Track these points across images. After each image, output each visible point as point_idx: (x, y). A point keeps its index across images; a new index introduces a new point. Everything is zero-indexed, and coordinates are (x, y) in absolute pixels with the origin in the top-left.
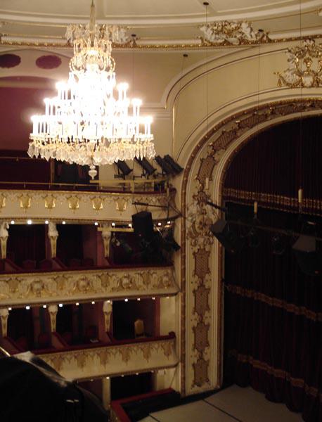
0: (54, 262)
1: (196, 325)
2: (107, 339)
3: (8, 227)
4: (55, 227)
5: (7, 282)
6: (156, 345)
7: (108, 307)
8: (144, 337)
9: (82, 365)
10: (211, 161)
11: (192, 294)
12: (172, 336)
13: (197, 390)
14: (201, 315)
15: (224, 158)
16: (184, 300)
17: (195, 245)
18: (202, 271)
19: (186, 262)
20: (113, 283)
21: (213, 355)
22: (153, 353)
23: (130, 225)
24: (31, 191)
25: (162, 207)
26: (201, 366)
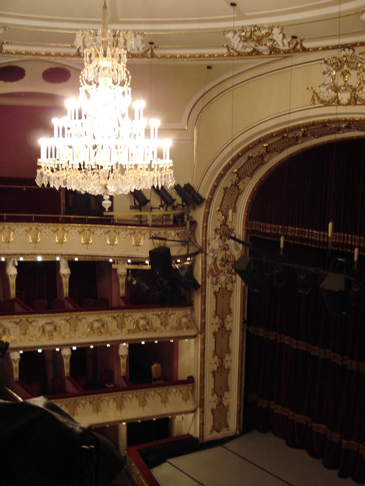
1: (216, 369)
3: (17, 264)
4: (66, 264)
6: (173, 390)
7: (123, 349)
8: (162, 381)
10: (234, 191)
12: (191, 380)
13: (216, 435)
15: (249, 187)
17: (216, 284)
18: (222, 312)
19: (206, 302)
20: (129, 324)
22: (171, 398)
26: (220, 411)
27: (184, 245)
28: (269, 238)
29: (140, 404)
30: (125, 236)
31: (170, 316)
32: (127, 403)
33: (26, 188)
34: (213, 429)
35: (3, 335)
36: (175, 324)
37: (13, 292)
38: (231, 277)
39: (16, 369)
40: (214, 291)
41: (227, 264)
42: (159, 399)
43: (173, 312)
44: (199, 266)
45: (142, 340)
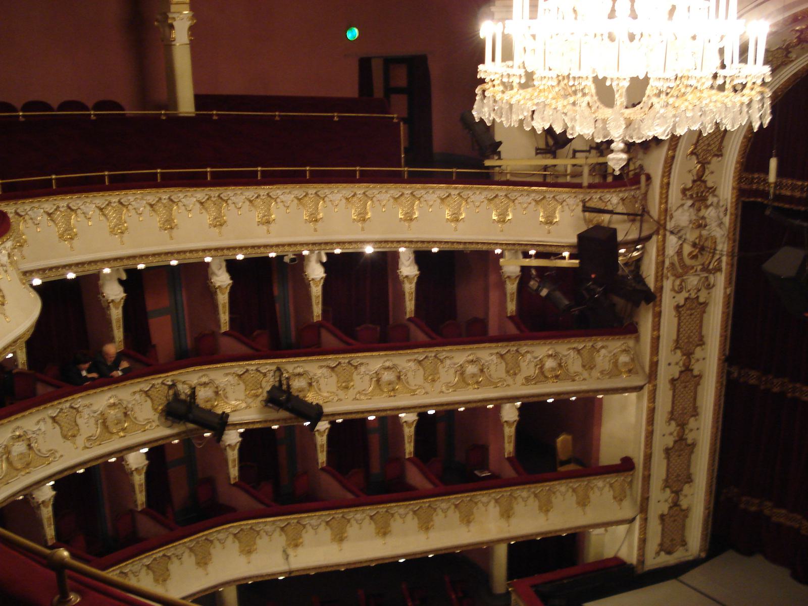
0: (412, 327)
1: (671, 444)
2: (509, 472)
3: (324, 259)
4: (412, 257)
5: (333, 369)
6: (599, 482)
7: (510, 413)
8: (572, 467)
9: (467, 519)
11: (669, 386)
12: (627, 465)
13: (665, 560)
14: (682, 425)
16: (653, 398)
17: (680, 291)
18: (690, 342)
19: (661, 325)
20: (528, 368)
21: (697, 499)
22: (594, 496)
23: (566, 254)
24: (372, 185)
25: (628, 214)
26: (675, 517)
27: (633, 221)
28: (787, 206)
29: (540, 508)
30: (525, 205)
31: (598, 351)
32: (519, 507)
33: (338, 117)
34: (661, 550)
35: (309, 391)
36: (607, 366)
37: (317, 310)
38: (707, 278)
39: (322, 446)
40: (676, 304)
41: (702, 254)
42: (574, 498)
43: (605, 344)
44: (651, 260)
45: (549, 395)
